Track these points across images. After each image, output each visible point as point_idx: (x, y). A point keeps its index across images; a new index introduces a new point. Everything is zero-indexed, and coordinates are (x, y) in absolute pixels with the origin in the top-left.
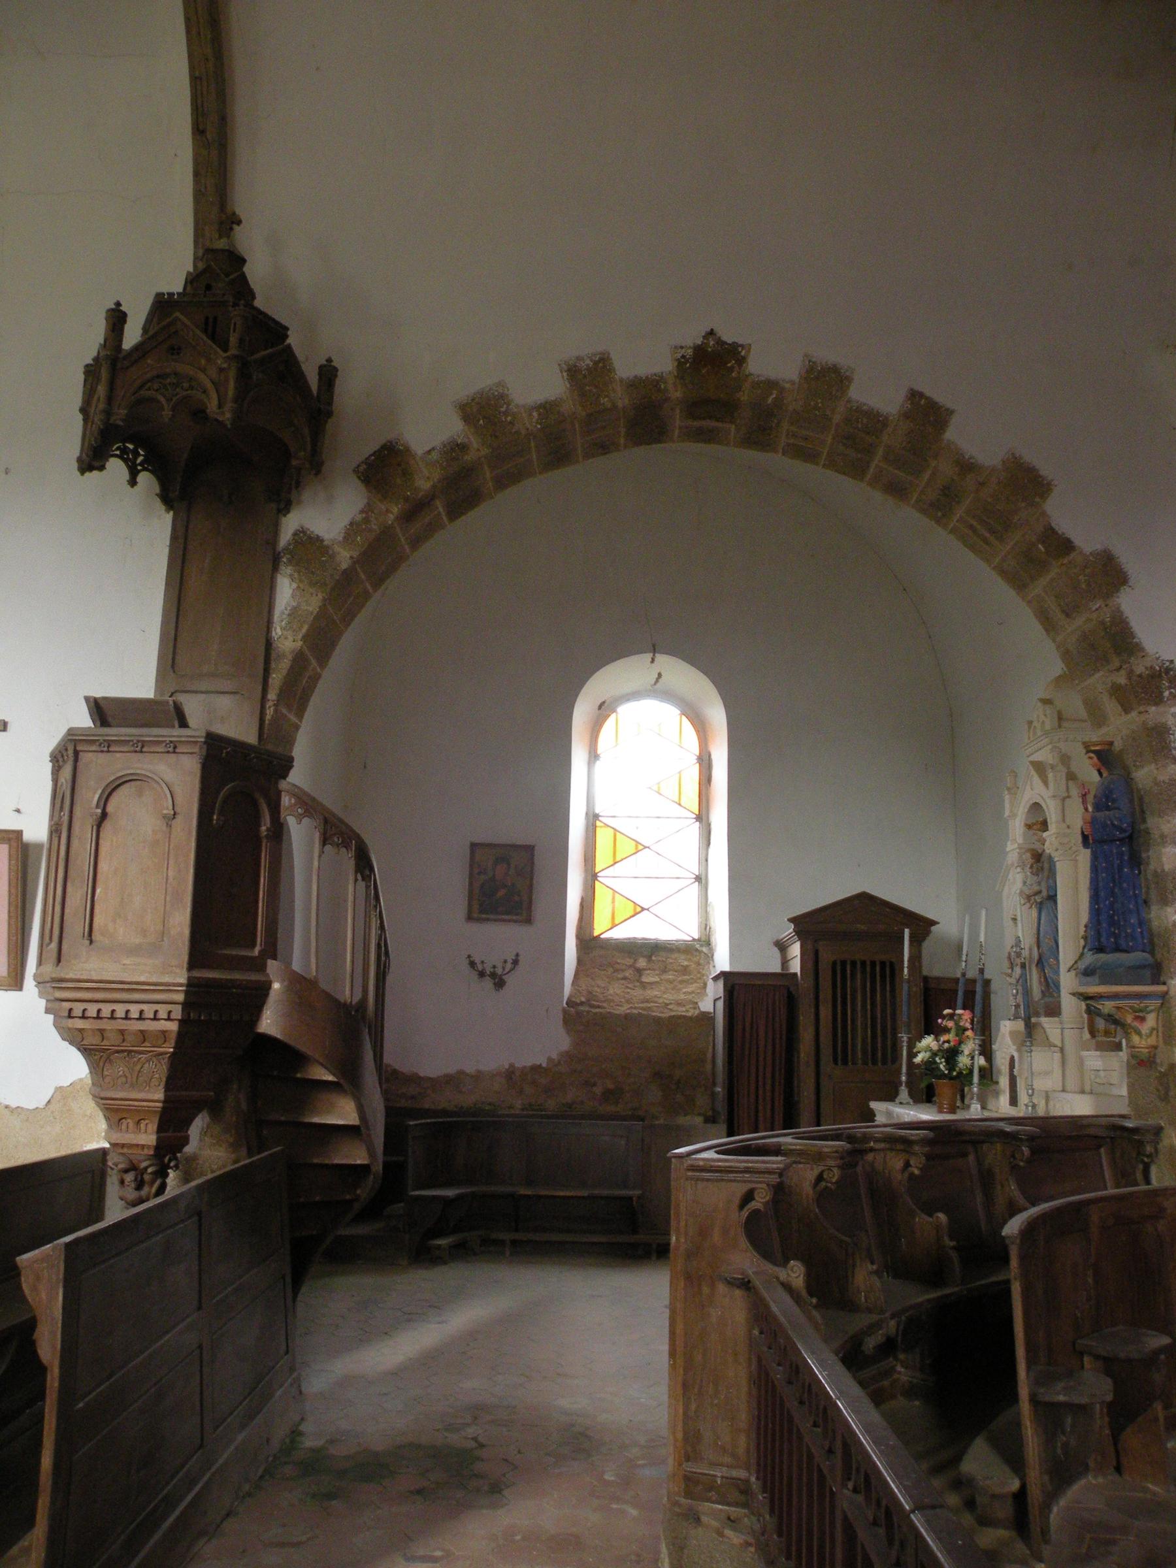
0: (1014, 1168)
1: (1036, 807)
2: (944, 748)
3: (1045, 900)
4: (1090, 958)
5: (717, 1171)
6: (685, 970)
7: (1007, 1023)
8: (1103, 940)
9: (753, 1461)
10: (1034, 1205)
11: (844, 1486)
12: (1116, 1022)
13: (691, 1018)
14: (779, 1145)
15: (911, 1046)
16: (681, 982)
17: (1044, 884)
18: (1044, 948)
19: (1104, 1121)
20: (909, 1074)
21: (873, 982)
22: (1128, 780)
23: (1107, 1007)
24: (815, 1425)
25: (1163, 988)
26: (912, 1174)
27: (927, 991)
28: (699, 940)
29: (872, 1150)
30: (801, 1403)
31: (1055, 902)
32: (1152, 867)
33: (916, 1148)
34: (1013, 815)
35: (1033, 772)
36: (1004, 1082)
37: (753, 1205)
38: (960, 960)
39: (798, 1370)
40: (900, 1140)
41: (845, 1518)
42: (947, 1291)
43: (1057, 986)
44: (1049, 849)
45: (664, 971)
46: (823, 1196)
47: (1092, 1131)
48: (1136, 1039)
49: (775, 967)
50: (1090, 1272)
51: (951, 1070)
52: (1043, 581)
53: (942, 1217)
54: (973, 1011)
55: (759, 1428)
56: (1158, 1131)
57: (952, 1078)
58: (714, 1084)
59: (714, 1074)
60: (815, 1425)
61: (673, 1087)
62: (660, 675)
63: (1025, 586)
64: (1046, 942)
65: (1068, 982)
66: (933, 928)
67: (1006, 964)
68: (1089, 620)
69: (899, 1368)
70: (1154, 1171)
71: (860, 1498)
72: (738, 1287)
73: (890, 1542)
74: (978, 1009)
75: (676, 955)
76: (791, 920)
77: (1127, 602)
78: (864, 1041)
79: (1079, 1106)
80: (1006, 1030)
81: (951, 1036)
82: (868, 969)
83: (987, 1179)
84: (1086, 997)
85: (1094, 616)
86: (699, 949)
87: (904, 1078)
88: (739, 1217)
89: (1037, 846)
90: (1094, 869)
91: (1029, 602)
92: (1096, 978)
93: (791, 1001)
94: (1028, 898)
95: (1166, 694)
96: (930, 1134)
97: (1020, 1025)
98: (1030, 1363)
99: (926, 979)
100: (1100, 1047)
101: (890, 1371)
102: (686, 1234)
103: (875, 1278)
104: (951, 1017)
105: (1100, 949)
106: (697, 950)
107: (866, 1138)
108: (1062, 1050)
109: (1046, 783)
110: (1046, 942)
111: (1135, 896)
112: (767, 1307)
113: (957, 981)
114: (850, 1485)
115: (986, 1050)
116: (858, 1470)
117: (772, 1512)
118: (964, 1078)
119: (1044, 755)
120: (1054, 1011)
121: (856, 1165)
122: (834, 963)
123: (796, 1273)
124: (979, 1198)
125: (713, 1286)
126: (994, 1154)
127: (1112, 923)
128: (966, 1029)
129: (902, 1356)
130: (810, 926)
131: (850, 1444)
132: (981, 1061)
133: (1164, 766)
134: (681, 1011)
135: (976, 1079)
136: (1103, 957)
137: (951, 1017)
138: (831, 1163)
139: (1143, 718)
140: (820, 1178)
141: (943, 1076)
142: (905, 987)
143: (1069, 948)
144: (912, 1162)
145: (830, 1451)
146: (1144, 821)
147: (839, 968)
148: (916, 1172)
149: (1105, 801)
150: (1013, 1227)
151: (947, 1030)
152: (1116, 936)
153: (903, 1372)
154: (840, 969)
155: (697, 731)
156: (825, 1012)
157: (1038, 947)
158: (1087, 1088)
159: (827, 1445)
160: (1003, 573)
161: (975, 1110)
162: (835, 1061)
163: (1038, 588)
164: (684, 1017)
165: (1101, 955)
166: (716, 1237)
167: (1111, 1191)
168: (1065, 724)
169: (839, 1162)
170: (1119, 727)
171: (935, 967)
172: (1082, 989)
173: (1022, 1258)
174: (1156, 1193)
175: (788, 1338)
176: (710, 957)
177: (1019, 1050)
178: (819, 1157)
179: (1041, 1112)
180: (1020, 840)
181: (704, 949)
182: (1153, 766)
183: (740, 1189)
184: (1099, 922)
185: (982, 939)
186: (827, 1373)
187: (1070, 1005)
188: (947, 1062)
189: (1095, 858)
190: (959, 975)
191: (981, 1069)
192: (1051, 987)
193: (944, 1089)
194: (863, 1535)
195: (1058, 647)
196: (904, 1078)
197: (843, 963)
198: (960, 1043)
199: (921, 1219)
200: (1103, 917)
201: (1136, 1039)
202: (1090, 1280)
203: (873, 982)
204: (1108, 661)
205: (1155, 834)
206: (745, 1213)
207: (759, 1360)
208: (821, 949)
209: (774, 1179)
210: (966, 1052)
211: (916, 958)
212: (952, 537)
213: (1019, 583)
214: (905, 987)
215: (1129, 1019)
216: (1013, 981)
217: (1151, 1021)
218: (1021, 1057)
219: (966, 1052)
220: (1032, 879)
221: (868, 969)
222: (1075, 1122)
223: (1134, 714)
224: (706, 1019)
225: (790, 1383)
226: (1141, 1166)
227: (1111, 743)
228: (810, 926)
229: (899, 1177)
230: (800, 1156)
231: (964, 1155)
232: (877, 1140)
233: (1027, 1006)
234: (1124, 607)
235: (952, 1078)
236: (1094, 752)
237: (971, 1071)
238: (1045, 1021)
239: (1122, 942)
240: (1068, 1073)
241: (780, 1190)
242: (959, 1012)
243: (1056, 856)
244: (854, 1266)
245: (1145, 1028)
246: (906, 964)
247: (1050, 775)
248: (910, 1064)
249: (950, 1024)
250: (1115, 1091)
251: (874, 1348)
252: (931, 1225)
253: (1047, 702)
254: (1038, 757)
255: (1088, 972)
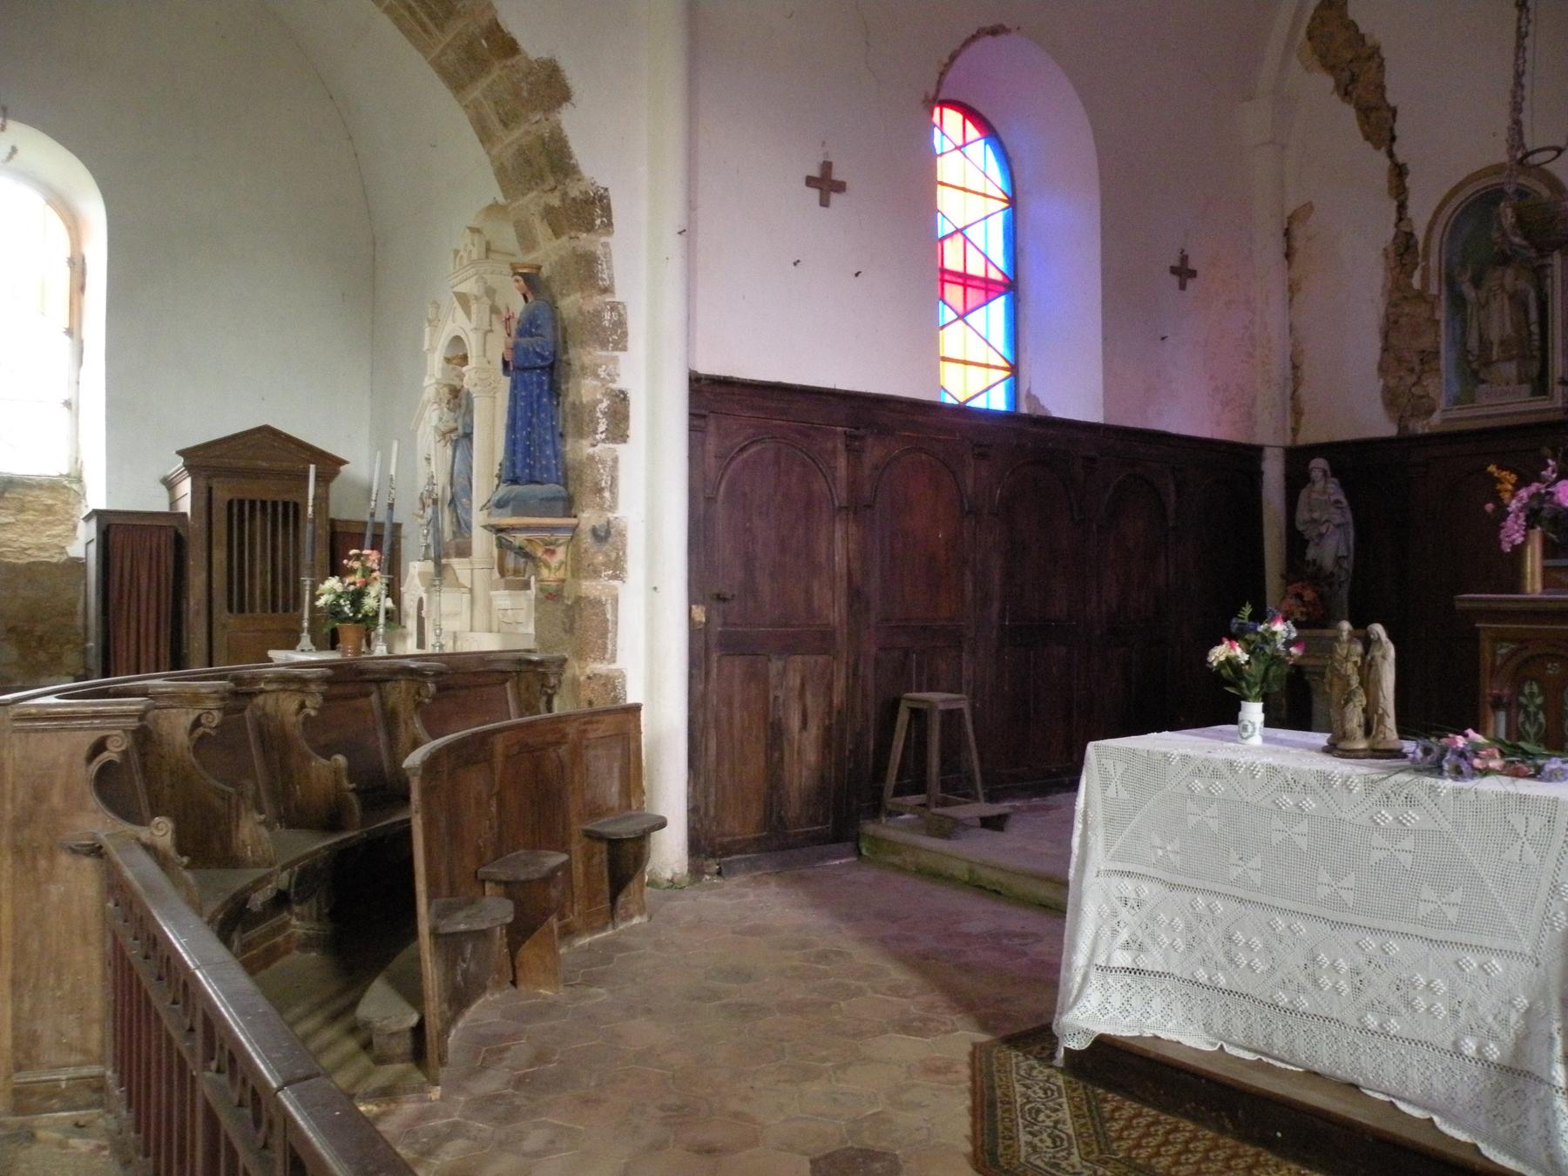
0: (419, 704)
1: (457, 340)
2: (364, 277)
3: (461, 438)
4: (504, 489)
5: (55, 719)
6: (49, 510)
7: (417, 564)
8: (518, 471)
9: (109, 1052)
10: (435, 738)
11: (206, 1068)
12: (527, 555)
13: (56, 565)
14: (146, 687)
15: (314, 587)
16: (45, 523)
17: (460, 421)
18: (457, 488)
19: (510, 656)
20: (312, 620)
21: (274, 525)
22: (553, 307)
23: (519, 539)
24: (175, 1002)
25: (573, 521)
26: (308, 716)
27: (333, 536)
28: (68, 476)
29: (262, 692)
30: (160, 978)
31: (471, 440)
32: (571, 398)
33: (313, 687)
34: (433, 349)
35: (456, 304)
36: (411, 625)
37: (105, 757)
38: (369, 499)
39: (155, 943)
40: (293, 681)
41: (207, 1104)
42: (346, 836)
43: (469, 527)
44: (467, 384)
45: (22, 510)
46: (201, 742)
47: (499, 666)
48: (545, 573)
49: (163, 507)
50: (494, 802)
51: (356, 612)
52: (483, 83)
53: (341, 759)
54: (380, 551)
55: (115, 1016)
56: (563, 662)
57: (358, 621)
58: (86, 640)
59: (86, 628)
60: (175, 1002)
61: (34, 644)
62: (14, 150)
63: (462, 87)
64: (460, 480)
65: (478, 518)
66: (342, 468)
67: (418, 505)
68: (528, 133)
69: (294, 922)
70: (556, 702)
71: (224, 1079)
72: (88, 855)
73: (257, 1123)
74: (386, 547)
75: (37, 492)
76: (181, 453)
77: (569, 120)
78: (263, 592)
79: (485, 642)
80: (415, 571)
81: (357, 578)
82: (269, 510)
83: (390, 719)
84: (499, 530)
85: (534, 127)
86: (64, 488)
87: (306, 624)
88: (86, 773)
89: (456, 382)
90: (513, 397)
91: (466, 106)
92: (509, 510)
93: (179, 543)
94: (444, 435)
95: (598, 222)
96: (329, 672)
97: (429, 566)
98: (431, 897)
99: (333, 522)
100: (509, 586)
101: (285, 926)
102: (13, 800)
103: (263, 831)
104: (358, 557)
105: (514, 481)
106: (65, 487)
107: (255, 679)
108: (471, 591)
109: (468, 314)
110: (460, 480)
111: (553, 427)
112: (120, 874)
113: (365, 523)
114: (213, 1065)
115: (393, 590)
116: (222, 1047)
117: (129, 1105)
118: (369, 621)
119: (469, 287)
120: (464, 551)
121: (242, 710)
122: (230, 503)
123: (162, 831)
124: (382, 736)
125: (51, 857)
126: (398, 693)
127: (528, 453)
128: (373, 571)
129: (297, 909)
130: (203, 461)
131: (211, 1024)
132: (389, 603)
133: (591, 296)
134: (43, 556)
135: (382, 620)
136: (517, 488)
137: (358, 557)
138: (211, 704)
139: (574, 243)
140: (197, 723)
141: (348, 619)
142: (309, 527)
143: (483, 486)
144: (308, 703)
145: (192, 1030)
146: (566, 351)
147: (235, 510)
148: (313, 713)
149: (528, 327)
150: (414, 759)
151: (352, 571)
152: (530, 467)
153: (298, 924)
154: (238, 511)
155: (69, 228)
156: (219, 555)
157: (452, 485)
158: (495, 628)
159: (187, 1022)
160: (442, 71)
161: (380, 650)
162: (230, 609)
163: (476, 92)
164: (48, 563)
165: (516, 487)
166: (56, 800)
167: (515, 720)
168: (492, 255)
169: (220, 704)
170: (549, 251)
171: (343, 508)
172: (495, 521)
173: (426, 792)
174: (559, 719)
175: (142, 905)
176: (80, 496)
177: (427, 591)
178: (196, 699)
179: (449, 649)
180: (438, 375)
181: (75, 487)
182: (579, 295)
183: (87, 739)
184: (514, 453)
185: (393, 472)
186: (188, 941)
187: (482, 542)
188: (352, 604)
189: (514, 387)
190: (367, 518)
191: (387, 612)
192: (462, 527)
193: (348, 633)
194: (226, 1122)
195: (492, 162)
196: (306, 624)
197: (241, 503)
198: (366, 584)
199: (319, 764)
200: (519, 449)
201: (545, 573)
202: (494, 809)
203: (274, 525)
204: (542, 178)
205: (576, 366)
206: (95, 766)
207: (115, 938)
208: (215, 486)
209: (133, 723)
210: (373, 594)
211: (322, 500)
212: (385, 16)
213: (457, 85)
214: (309, 527)
215: (539, 553)
216: (424, 521)
217: (561, 553)
218: (429, 598)
219: (373, 594)
220: (448, 415)
221: (269, 510)
222: (483, 657)
223: (564, 238)
224: (78, 565)
225: (147, 957)
226: (544, 698)
227: (539, 268)
228: (203, 461)
229: (294, 719)
230: (179, 701)
231: (368, 695)
232: (269, 681)
233: (438, 542)
234: (564, 125)
235: (358, 621)
236: (522, 275)
237: (377, 615)
238: (457, 563)
239: (537, 473)
240: (476, 613)
241: (144, 737)
242: (366, 552)
243: (475, 392)
244: (238, 818)
245: (554, 561)
246: (310, 502)
247: (474, 308)
248: (313, 608)
249: (356, 565)
250: (522, 630)
251: (263, 904)
252: (327, 771)
253: (474, 230)
254: (462, 288)
255: (501, 504)
